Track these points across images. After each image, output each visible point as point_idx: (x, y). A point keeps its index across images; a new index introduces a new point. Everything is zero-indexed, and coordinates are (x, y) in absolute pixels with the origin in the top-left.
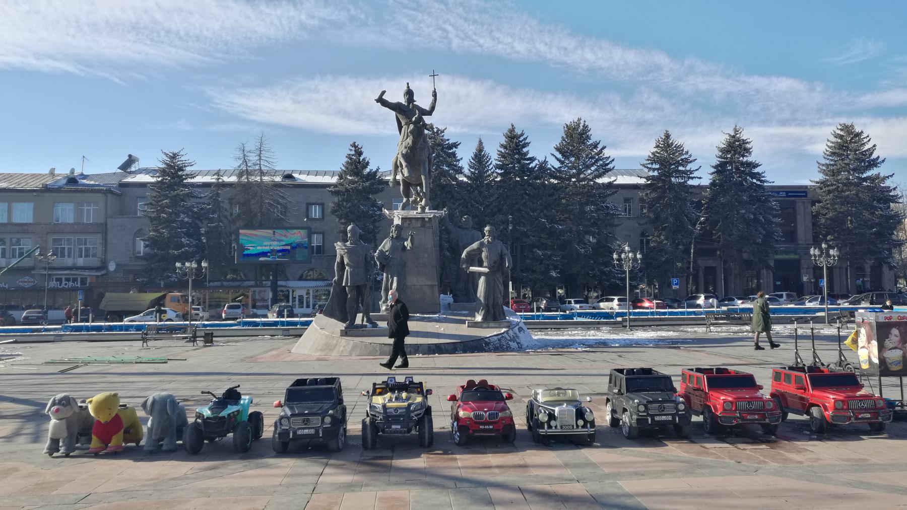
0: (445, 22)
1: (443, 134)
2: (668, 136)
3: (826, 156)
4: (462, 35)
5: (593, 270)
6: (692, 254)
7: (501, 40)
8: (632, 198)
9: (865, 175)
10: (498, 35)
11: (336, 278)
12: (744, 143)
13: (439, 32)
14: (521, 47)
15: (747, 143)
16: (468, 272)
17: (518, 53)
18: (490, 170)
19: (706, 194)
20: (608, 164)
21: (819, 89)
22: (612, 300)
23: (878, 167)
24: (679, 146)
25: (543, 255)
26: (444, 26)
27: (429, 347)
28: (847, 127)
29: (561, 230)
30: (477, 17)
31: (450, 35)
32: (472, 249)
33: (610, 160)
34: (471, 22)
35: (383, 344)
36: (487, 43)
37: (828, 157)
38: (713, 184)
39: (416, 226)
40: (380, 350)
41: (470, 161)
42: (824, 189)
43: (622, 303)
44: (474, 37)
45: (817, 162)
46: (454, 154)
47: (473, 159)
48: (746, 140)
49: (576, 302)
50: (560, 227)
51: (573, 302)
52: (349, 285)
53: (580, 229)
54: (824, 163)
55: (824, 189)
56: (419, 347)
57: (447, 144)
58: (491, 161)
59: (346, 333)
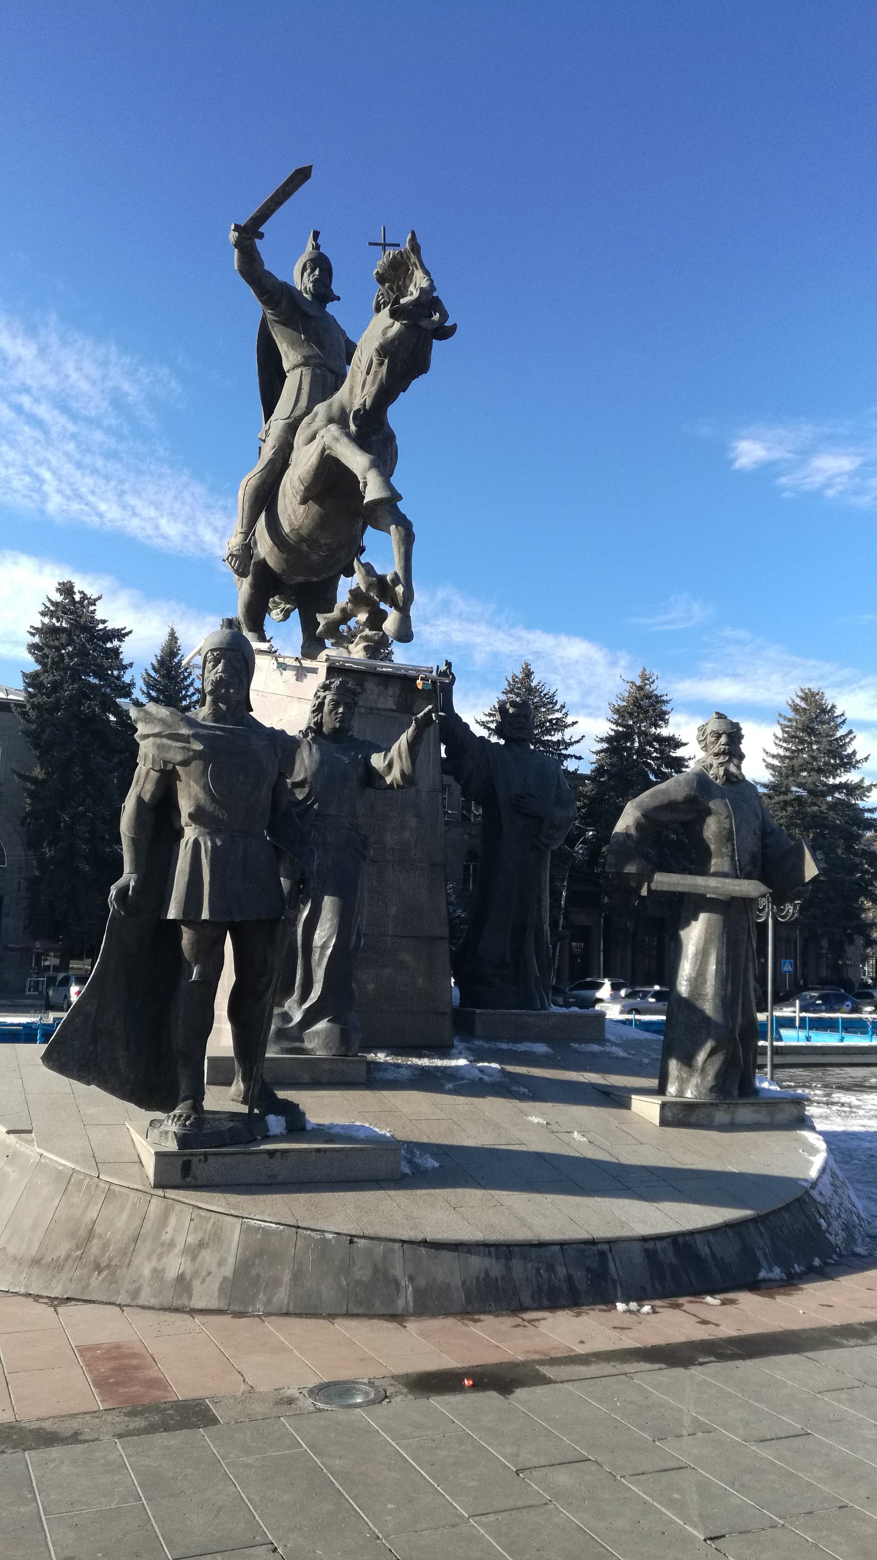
0: (40, 463)
1: (92, 608)
2: (528, 674)
3: (777, 742)
4: (68, 492)
6: (563, 899)
7: (137, 511)
9: (837, 781)
10: (132, 500)
11: (128, 877)
12: (658, 702)
13: (27, 479)
14: (171, 529)
15: (664, 702)
16: (644, 892)
17: (165, 537)
18: (190, 697)
19: (586, 789)
21: (623, 663)
23: (858, 768)
24: (545, 695)
26: (37, 470)
27: (650, 1255)
28: (813, 695)
30: (100, 463)
31: (46, 487)
32: (664, 800)
34: (87, 471)
35: (424, 1243)
36: (111, 511)
37: (781, 743)
38: (599, 771)
39: (381, 705)
40: (411, 1279)
41: (149, 675)
42: (777, 799)
44: (91, 498)
45: (764, 750)
46: (116, 652)
47: (154, 668)
48: (661, 696)
52: (205, 915)
54: (776, 754)
55: (777, 799)
56: (602, 1254)
57: (100, 630)
58: (191, 678)
59: (186, 1167)
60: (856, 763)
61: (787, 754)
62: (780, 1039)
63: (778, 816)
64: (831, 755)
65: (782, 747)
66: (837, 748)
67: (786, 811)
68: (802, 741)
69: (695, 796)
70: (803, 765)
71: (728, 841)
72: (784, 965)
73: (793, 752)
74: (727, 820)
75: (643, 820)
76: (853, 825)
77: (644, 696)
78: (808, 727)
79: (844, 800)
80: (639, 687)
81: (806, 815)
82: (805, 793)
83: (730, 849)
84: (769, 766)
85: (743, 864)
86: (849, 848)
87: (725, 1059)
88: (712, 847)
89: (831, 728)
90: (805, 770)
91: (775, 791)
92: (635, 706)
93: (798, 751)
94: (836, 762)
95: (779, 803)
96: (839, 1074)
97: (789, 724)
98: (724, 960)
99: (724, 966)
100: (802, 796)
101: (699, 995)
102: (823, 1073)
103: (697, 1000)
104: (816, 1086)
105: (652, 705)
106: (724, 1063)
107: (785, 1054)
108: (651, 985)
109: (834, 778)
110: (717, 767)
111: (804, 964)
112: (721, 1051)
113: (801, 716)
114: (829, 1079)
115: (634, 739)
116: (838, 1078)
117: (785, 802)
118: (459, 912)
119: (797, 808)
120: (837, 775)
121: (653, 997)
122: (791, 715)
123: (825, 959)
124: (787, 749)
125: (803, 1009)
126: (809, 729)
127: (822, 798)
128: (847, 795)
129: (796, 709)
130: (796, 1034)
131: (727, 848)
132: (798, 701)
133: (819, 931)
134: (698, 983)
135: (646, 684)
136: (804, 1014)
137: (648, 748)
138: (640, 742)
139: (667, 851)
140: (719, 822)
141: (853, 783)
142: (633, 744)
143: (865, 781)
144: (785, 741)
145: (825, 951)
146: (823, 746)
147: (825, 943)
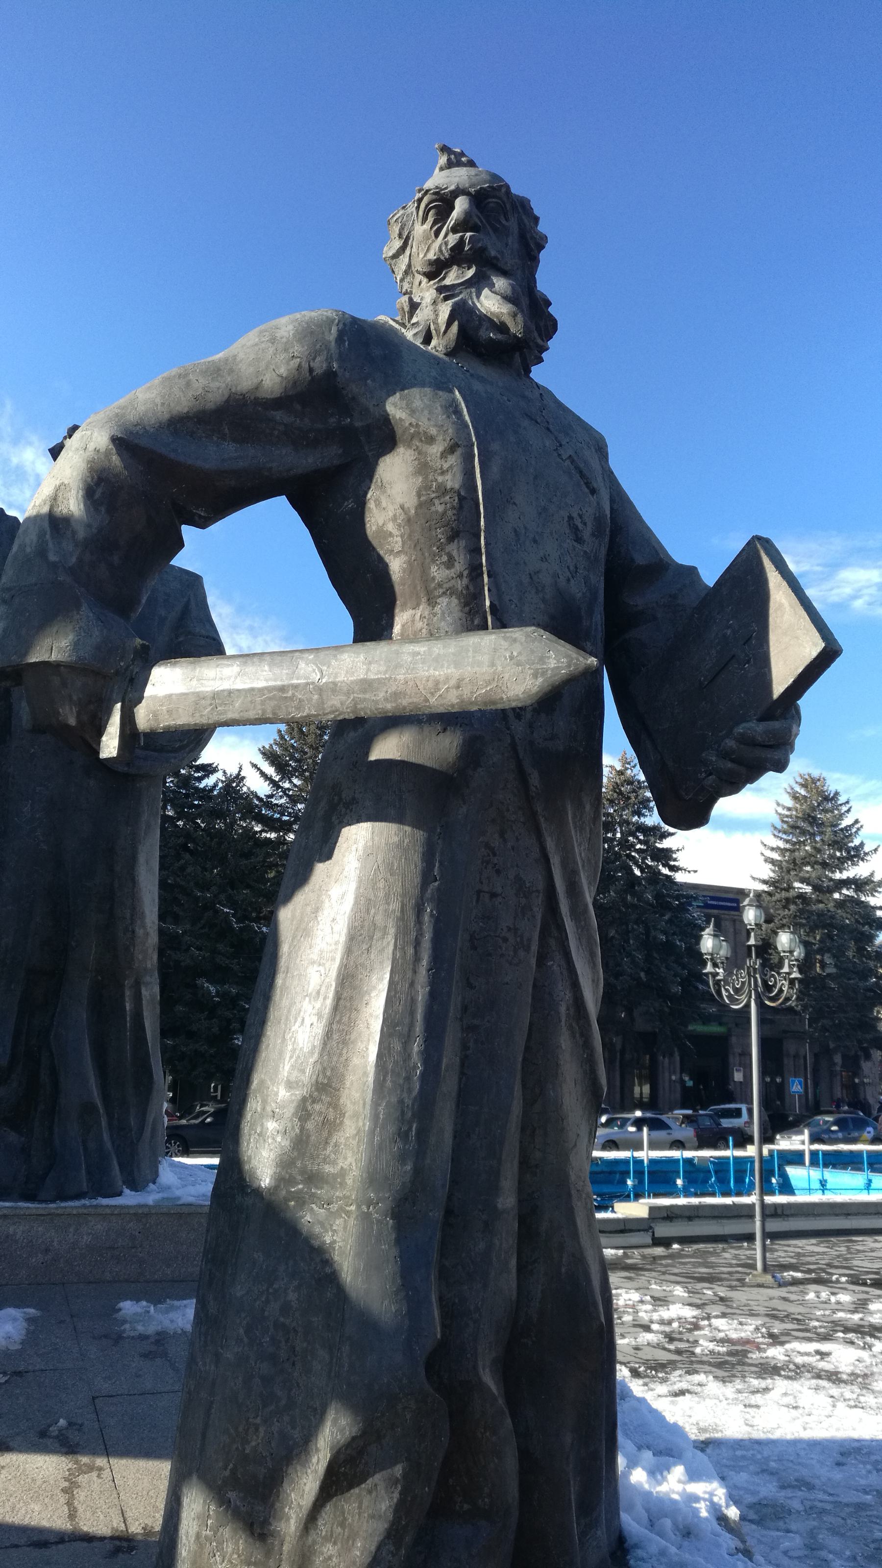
9: (845, 875)
25: (218, 994)
28: (814, 781)
37: (780, 835)
45: (762, 843)
60: (865, 856)
61: (788, 846)
62: (786, 1187)
63: (779, 915)
64: (836, 846)
65: (781, 839)
66: (843, 839)
67: (789, 910)
68: (803, 832)
69: (330, 374)
70: (805, 858)
72: (793, 1086)
73: (794, 844)
74: (453, 460)
75: (115, 459)
76: (863, 925)
77: (625, 781)
78: (809, 816)
79: (853, 897)
80: (619, 771)
81: (811, 912)
82: (808, 889)
83: (460, 566)
84: (768, 860)
86: (861, 950)
87: (401, 1508)
88: (396, 566)
89: (835, 816)
90: (808, 864)
91: (776, 887)
92: (615, 792)
93: (799, 842)
94: (842, 855)
95: (780, 901)
96: (872, 1250)
97: (788, 813)
98: (419, 1028)
99: (416, 1047)
100: (806, 893)
101: (313, 1178)
102: (848, 1248)
103: (302, 1201)
104: (838, 1281)
105: (634, 791)
106: (393, 1534)
107: (787, 1216)
108: (632, 1110)
109: (841, 872)
110: (434, 303)
111: (816, 1084)
112: (380, 1467)
113: (801, 805)
114: (861, 1263)
115: (615, 830)
116: (873, 1259)
117: (787, 900)
119: (801, 906)
120: (845, 869)
121: (632, 1125)
122: (789, 803)
123: (839, 1077)
124: (787, 841)
125: (814, 1139)
126: (811, 819)
127: (828, 895)
128: (856, 891)
129: (795, 797)
130: (807, 1174)
131: (450, 564)
132: (798, 789)
133: (832, 1045)
134: (310, 1125)
135: (627, 769)
136: (816, 1147)
137: (631, 838)
138: (622, 833)
139: (655, 955)
140: (423, 468)
141: (862, 878)
142: (614, 835)
143: (875, 874)
144: (785, 833)
145: (838, 1068)
146: (827, 837)
147: (838, 1059)
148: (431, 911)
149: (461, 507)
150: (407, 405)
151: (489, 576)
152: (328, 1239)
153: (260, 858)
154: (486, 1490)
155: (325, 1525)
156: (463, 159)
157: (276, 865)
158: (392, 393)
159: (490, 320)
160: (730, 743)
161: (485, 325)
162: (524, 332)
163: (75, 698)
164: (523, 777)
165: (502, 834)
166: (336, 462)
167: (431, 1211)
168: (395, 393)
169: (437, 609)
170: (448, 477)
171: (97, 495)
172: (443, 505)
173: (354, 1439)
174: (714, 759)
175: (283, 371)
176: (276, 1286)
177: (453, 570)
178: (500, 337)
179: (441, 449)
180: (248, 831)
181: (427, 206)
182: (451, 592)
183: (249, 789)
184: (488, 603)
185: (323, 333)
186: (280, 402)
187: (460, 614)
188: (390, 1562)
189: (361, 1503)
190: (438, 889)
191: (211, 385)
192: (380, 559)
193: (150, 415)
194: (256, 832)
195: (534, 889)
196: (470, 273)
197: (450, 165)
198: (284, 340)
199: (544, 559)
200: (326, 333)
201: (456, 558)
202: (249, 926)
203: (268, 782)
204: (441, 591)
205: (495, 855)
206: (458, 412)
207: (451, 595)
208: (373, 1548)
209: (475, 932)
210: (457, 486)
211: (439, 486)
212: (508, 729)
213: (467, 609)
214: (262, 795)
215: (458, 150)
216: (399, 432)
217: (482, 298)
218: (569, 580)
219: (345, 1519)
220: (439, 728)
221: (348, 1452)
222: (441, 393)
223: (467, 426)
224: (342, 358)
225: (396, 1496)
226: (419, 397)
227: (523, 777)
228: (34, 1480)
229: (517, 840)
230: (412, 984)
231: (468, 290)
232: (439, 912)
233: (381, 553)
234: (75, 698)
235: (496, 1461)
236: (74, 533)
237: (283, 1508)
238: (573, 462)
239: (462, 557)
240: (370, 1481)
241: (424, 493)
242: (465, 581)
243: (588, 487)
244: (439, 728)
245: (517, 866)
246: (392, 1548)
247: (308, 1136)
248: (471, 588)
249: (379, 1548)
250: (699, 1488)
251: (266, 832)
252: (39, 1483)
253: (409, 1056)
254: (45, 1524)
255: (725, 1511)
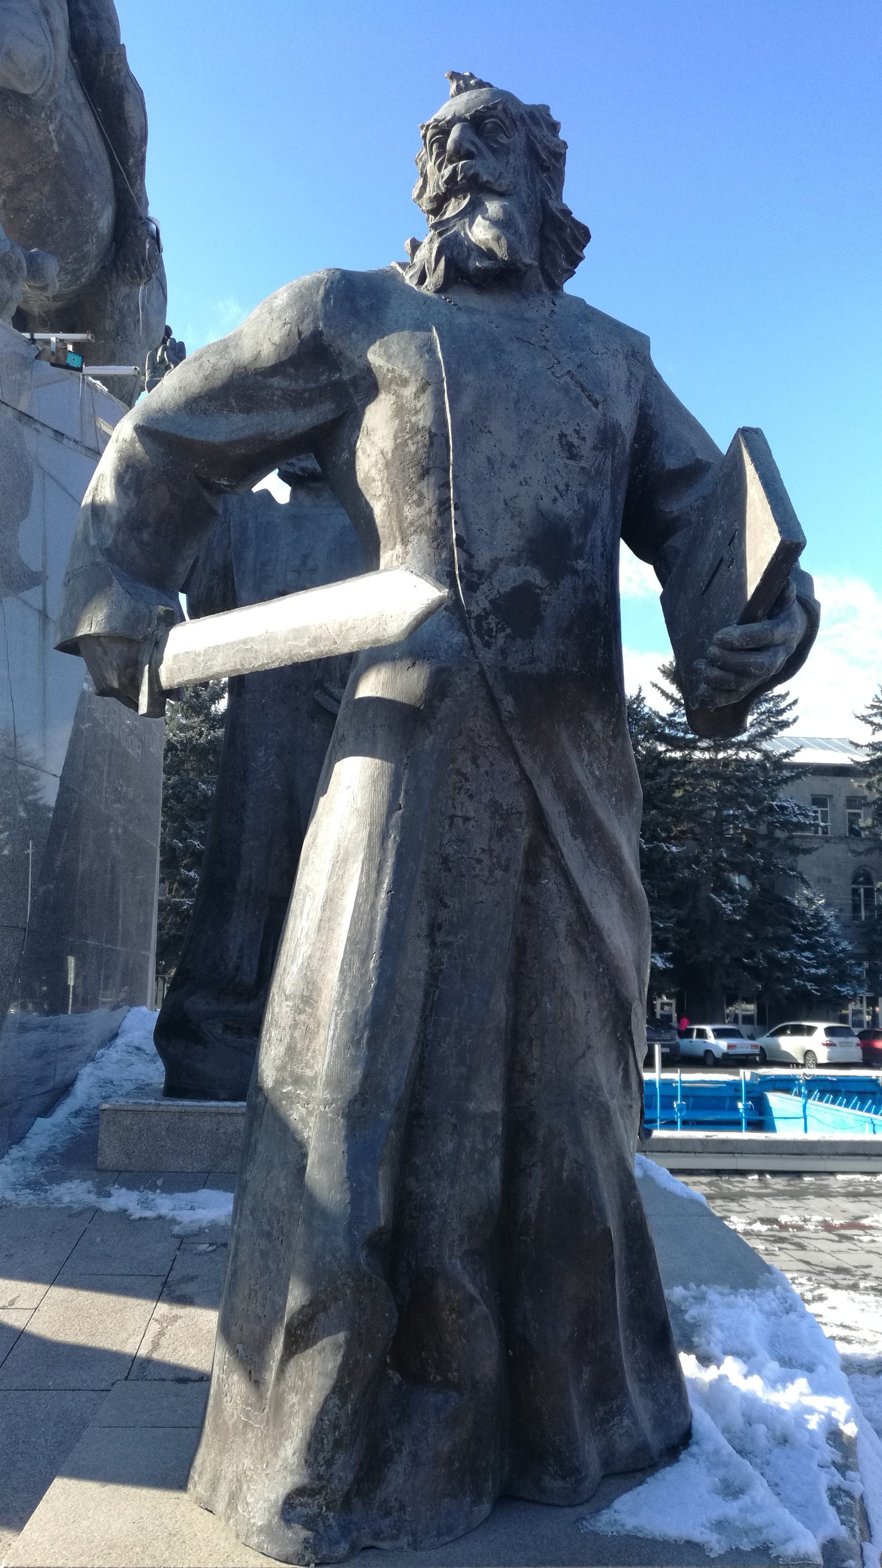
5: (751, 955)
8: (831, 796)
20: (783, 711)
22: (810, 1031)
29: (675, 858)
33: (789, 700)
43: (836, 1040)
49: (719, 1034)
50: (674, 849)
51: (710, 1034)
53: (721, 856)
69: (317, 334)
71: (425, 473)
85: (483, 559)
87: (346, 1370)
88: (378, 508)
98: (376, 944)
118: (845, 944)
131: (419, 503)
134: (297, 1034)
140: (400, 410)
148: (395, 838)
149: (431, 444)
150: (385, 352)
151: (455, 509)
152: (306, 1135)
153: (665, 778)
154: (454, 1365)
155: (290, 1377)
156: (472, 82)
157: (684, 784)
158: (372, 342)
159: (479, 249)
160: (713, 650)
161: (474, 254)
162: (508, 254)
163: (114, 664)
164: (494, 703)
165: (474, 760)
166: (330, 417)
167: (382, 1112)
168: (375, 342)
169: (409, 547)
170: (421, 416)
171: (126, 481)
172: (415, 445)
173: (303, 1307)
174: (703, 667)
175: (277, 338)
176: (272, 1175)
177: (422, 508)
178: (486, 264)
179: (414, 390)
180: (651, 751)
181: (431, 138)
182: (421, 529)
183: (650, 709)
184: (454, 536)
185: (312, 295)
186: (276, 369)
187: (429, 550)
188: (336, 1413)
189: (314, 1362)
190: (402, 817)
191: (219, 363)
192: (367, 504)
193: (170, 399)
194: (661, 753)
195: (514, 811)
196: (465, 202)
197: (459, 91)
198: (279, 309)
199: (524, 483)
200: (314, 295)
201: (426, 495)
202: (657, 846)
203: (670, 701)
204: (412, 529)
205: (467, 780)
206: (432, 351)
207: (421, 532)
208: (322, 1400)
209: (449, 854)
210: (428, 424)
211: (413, 426)
212: (476, 658)
213: (435, 544)
214: (664, 714)
215: (467, 74)
216: (380, 378)
217: (474, 227)
218: (555, 500)
219: (303, 1374)
220: (409, 663)
221: (300, 1317)
222: (418, 334)
223: (439, 362)
224: (327, 317)
225: (339, 1358)
226: (396, 341)
227: (494, 703)
228: (200, 1330)
229: (492, 764)
230: (373, 906)
231: (462, 221)
232: (402, 839)
233: (368, 498)
234: (114, 664)
235: (464, 1341)
236: (110, 517)
237: (269, 1362)
238: (572, 377)
239: (431, 493)
240: (319, 1344)
241: (400, 435)
242: (434, 516)
243: (590, 400)
244: (409, 663)
245: (492, 790)
246: (338, 1402)
247: (296, 1043)
248: (439, 522)
249: (326, 1400)
250: (822, 1403)
251: (671, 751)
252: (204, 1332)
253: (367, 971)
254: (194, 1365)
255: (842, 1427)
